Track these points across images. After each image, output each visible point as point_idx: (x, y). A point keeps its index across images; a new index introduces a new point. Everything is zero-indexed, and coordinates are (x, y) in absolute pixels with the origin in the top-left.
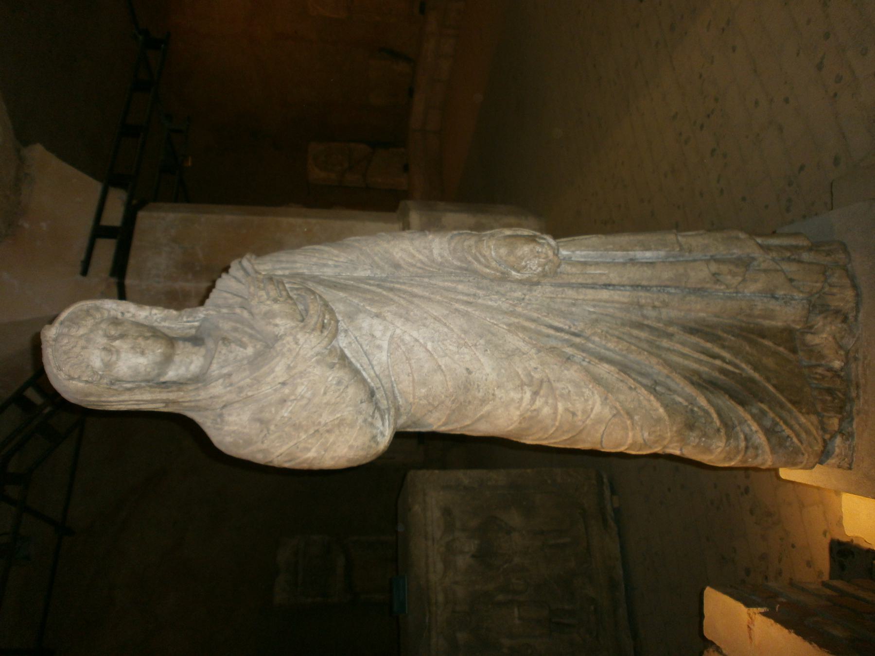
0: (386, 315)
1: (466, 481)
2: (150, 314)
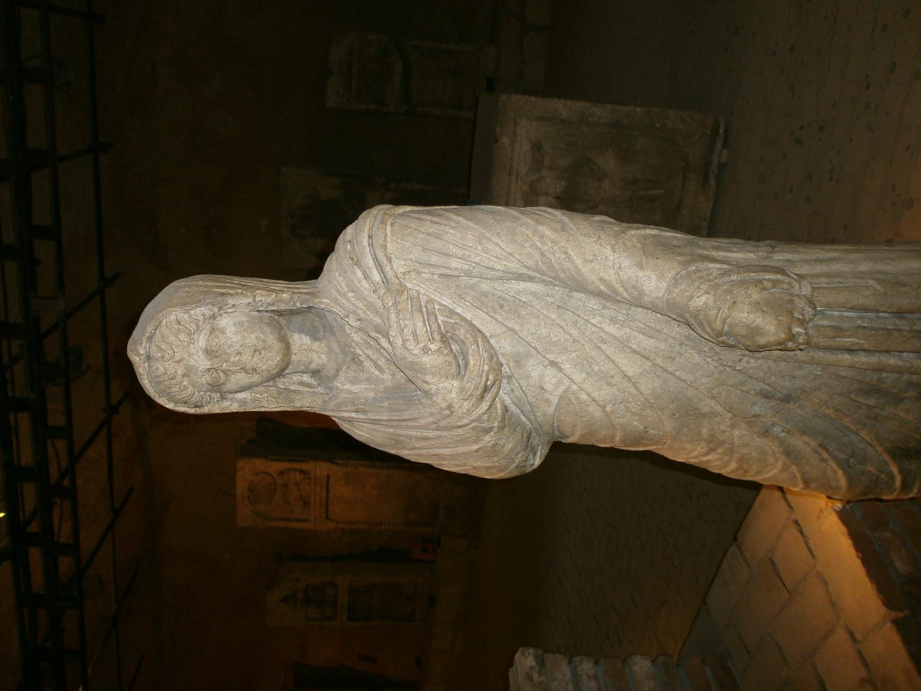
1: (565, 114)
2: (254, 300)
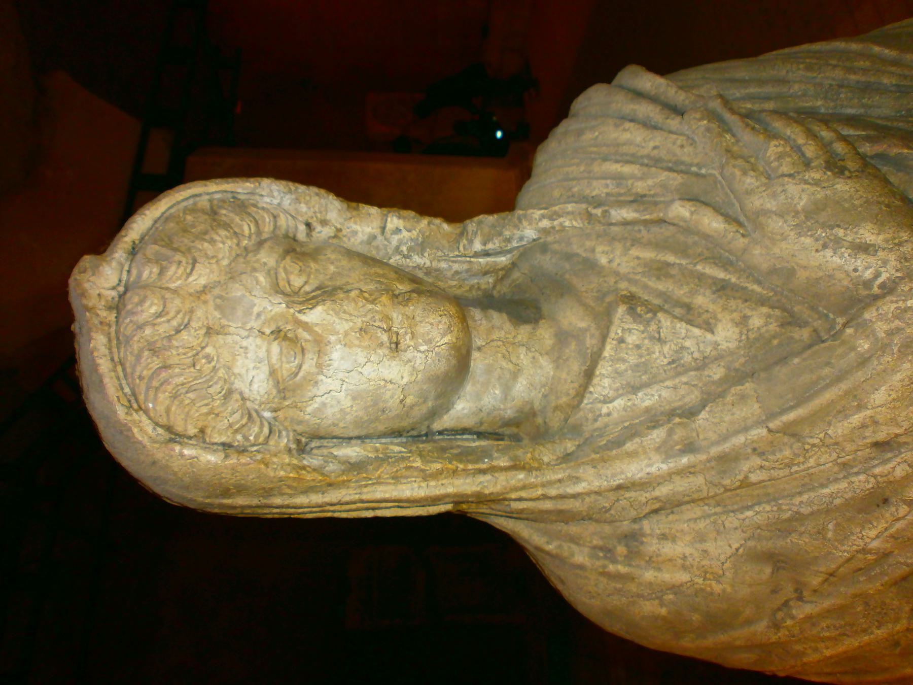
2: (383, 229)
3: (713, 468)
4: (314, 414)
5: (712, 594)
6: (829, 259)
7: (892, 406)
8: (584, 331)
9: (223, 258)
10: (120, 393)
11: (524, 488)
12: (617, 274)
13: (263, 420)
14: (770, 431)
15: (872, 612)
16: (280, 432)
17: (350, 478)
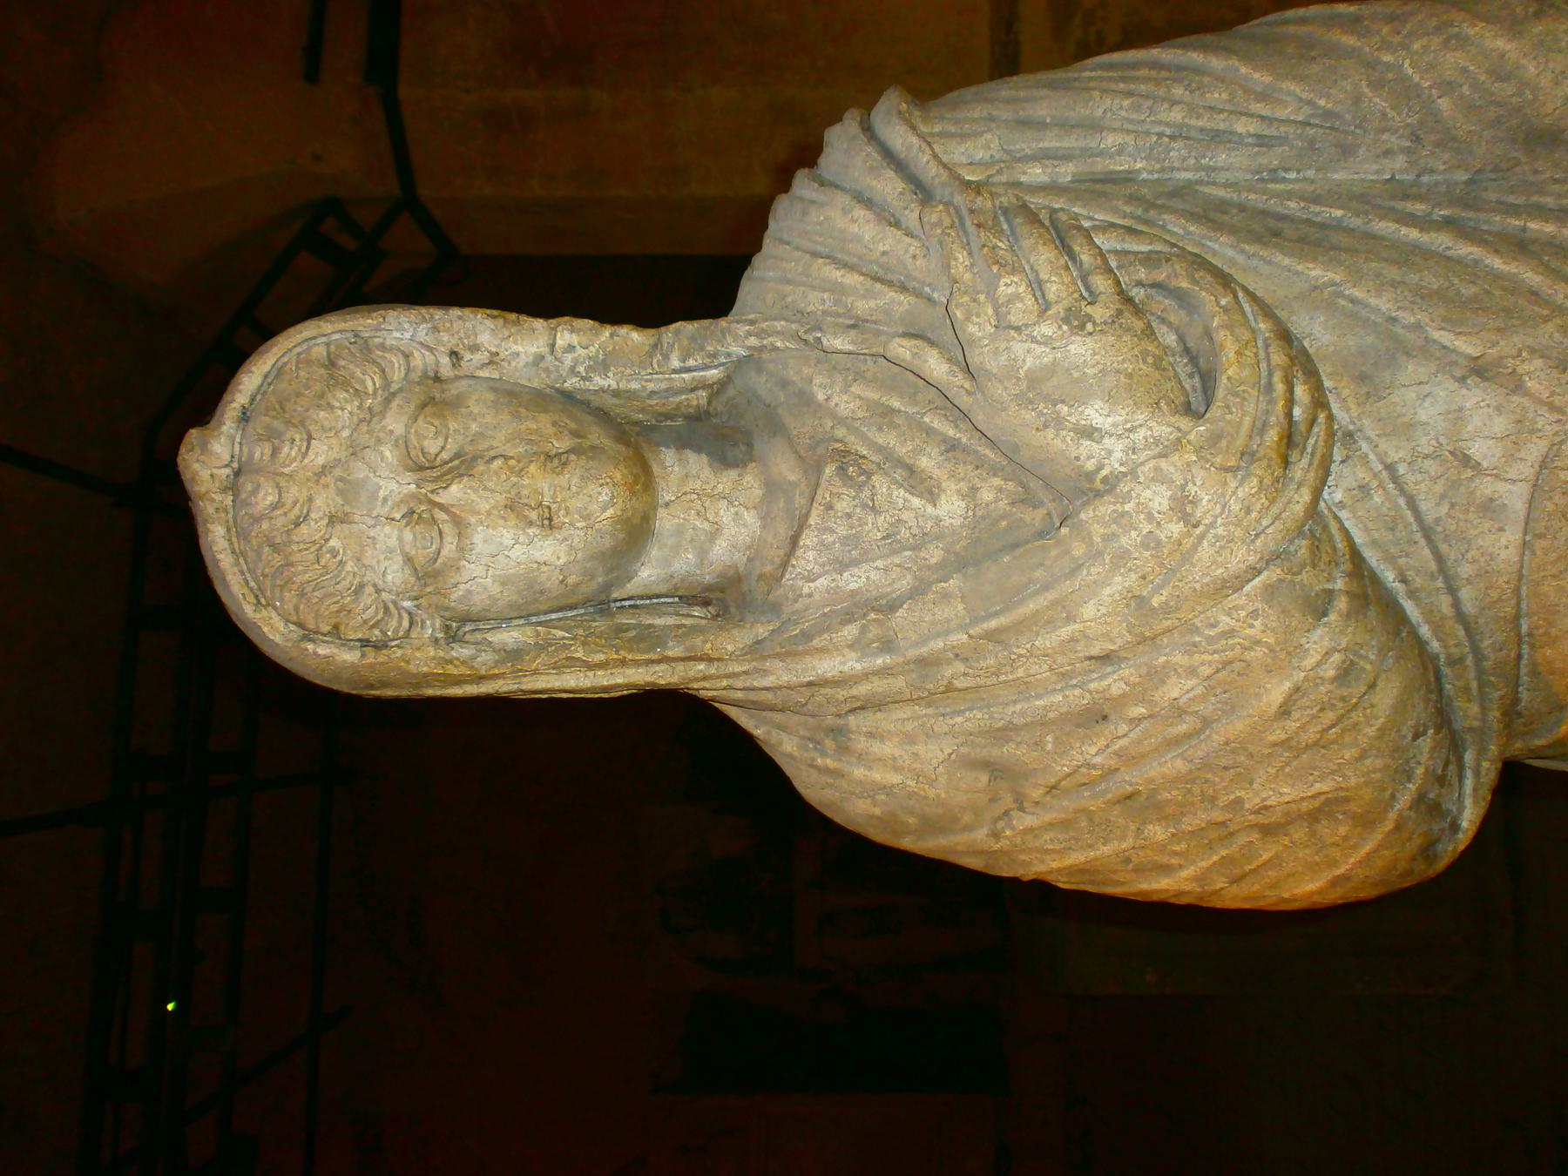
0: (1523, 368)
2: (553, 346)
3: (913, 671)
4: (460, 600)
5: (926, 798)
6: (1049, 441)
7: (1102, 621)
8: (795, 484)
9: (343, 427)
10: (246, 590)
11: (704, 678)
12: (833, 416)
13: (402, 611)
14: (970, 637)
15: (1097, 829)
16: (423, 622)
17: (502, 671)
